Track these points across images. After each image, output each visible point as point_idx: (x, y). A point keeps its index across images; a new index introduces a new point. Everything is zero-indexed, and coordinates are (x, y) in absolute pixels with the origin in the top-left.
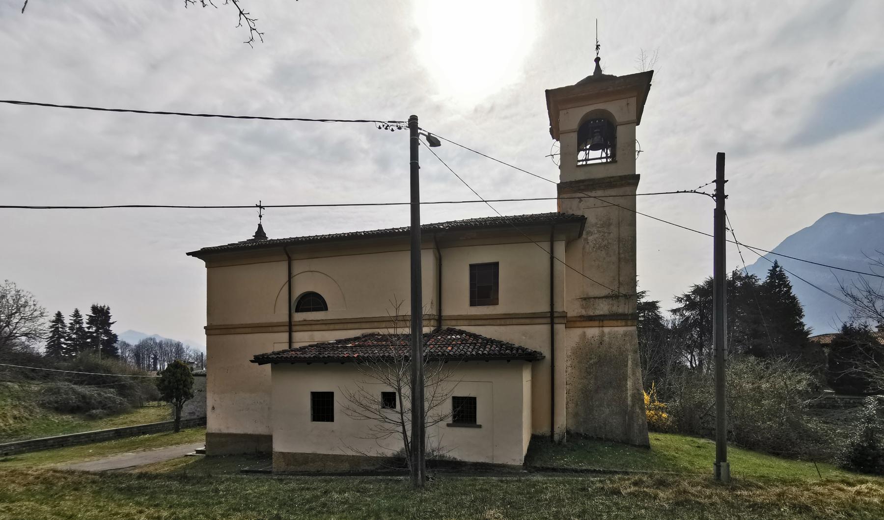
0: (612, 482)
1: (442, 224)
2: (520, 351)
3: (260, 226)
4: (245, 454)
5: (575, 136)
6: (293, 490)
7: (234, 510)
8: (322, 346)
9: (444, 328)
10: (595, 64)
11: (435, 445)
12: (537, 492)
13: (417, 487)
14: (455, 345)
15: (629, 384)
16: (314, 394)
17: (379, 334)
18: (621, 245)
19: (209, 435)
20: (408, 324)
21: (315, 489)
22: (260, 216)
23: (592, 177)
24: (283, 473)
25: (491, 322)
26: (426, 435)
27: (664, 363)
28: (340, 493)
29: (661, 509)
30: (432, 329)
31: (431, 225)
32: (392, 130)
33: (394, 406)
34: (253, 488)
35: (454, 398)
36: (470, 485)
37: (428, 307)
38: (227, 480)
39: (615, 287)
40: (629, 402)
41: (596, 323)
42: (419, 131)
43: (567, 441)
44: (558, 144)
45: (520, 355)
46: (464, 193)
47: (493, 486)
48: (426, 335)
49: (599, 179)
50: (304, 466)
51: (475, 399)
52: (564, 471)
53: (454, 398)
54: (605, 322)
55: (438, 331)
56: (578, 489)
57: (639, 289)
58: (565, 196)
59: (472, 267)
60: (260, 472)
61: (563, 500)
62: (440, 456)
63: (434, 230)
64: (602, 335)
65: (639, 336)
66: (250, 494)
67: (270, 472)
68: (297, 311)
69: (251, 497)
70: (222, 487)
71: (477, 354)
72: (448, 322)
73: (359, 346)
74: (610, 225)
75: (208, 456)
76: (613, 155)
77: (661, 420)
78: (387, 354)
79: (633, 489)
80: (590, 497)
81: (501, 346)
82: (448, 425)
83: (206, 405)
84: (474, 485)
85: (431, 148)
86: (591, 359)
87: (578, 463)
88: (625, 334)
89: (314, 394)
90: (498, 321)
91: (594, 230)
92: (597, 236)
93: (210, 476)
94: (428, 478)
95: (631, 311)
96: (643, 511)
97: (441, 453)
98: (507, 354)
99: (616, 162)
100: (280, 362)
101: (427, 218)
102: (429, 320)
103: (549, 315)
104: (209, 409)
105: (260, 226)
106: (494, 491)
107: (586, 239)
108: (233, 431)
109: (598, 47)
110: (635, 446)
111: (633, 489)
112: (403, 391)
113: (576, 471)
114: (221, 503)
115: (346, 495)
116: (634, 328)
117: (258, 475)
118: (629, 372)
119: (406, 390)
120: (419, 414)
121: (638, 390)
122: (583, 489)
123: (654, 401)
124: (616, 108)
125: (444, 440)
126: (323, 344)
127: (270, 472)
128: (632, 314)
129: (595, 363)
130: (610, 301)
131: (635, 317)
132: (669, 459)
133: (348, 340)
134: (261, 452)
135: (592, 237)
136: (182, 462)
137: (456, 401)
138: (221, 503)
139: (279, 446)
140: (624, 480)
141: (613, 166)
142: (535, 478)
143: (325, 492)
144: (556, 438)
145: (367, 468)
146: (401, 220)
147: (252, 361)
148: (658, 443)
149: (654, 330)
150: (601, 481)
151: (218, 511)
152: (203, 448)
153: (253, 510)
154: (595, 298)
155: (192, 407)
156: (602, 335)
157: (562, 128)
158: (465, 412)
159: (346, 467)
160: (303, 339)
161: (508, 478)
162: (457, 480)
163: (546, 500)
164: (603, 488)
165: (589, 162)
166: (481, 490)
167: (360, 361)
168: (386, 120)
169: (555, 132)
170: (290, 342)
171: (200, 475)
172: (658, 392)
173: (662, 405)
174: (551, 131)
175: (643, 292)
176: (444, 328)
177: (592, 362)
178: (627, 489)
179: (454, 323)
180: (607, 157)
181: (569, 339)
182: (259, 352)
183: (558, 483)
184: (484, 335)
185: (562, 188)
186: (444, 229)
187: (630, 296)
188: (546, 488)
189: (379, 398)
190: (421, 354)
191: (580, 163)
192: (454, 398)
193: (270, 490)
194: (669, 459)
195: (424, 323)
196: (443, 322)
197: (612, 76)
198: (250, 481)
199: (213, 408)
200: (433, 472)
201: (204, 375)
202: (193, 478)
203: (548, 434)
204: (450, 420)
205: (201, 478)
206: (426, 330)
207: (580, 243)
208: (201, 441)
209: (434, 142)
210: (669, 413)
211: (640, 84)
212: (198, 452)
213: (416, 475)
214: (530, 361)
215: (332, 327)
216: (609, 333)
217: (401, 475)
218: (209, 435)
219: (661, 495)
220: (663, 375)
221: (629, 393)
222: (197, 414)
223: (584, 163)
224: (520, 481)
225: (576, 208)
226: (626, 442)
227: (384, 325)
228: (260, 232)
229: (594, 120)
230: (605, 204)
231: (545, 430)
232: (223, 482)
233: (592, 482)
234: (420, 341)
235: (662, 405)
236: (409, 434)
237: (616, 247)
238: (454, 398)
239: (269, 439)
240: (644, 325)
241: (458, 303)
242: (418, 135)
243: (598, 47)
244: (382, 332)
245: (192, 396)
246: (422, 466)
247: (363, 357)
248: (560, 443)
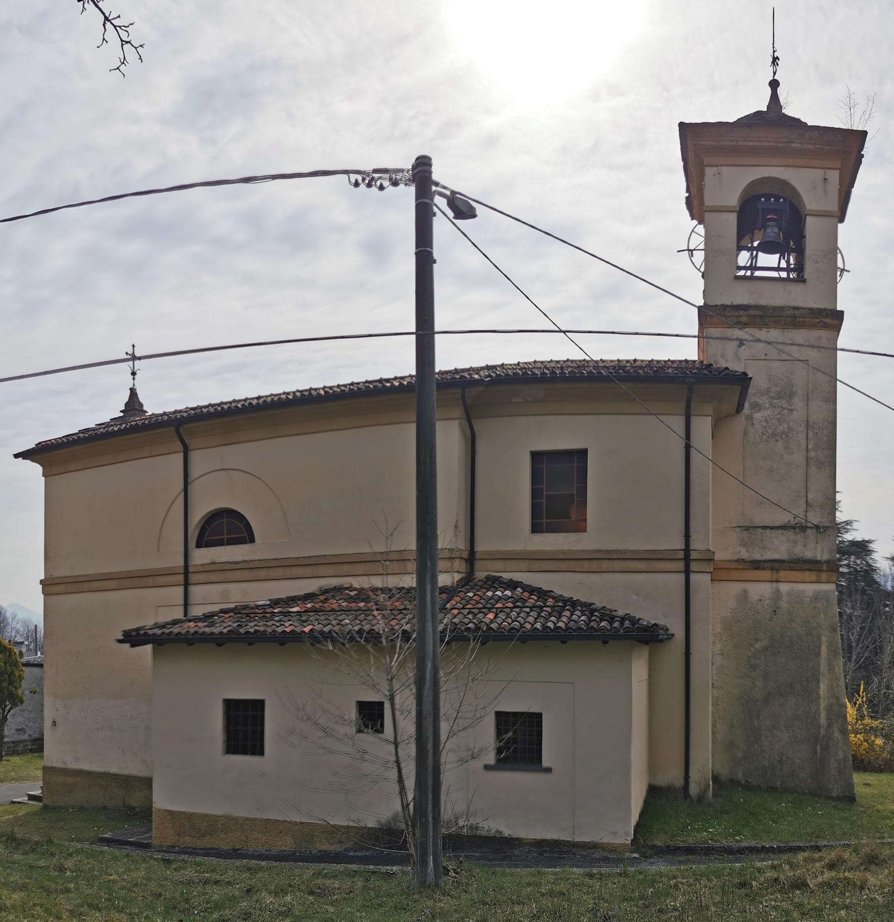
0: (793, 866)
1: (477, 370)
2: (627, 623)
3: (133, 393)
4: (105, 808)
5: (732, 219)
6: (190, 883)
7: (90, 906)
8: (242, 612)
9: (480, 575)
10: (768, 91)
11: (461, 807)
12: (657, 894)
13: (425, 886)
14: (501, 610)
15: (823, 686)
16: (229, 704)
17: (351, 588)
18: (811, 434)
19: (46, 769)
20: (412, 566)
21: (228, 883)
22: (134, 374)
23: (763, 302)
24: (171, 849)
25: (572, 565)
26: (444, 788)
27: (878, 650)
28: (276, 894)
29: (871, 905)
30: (457, 577)
31: (456, 371)
32: (381, 188)
33: (380, 730)
34: (121, 870)
35: (498, 714)
36: (529, 884)
37: (447, 537)
38: (78, 852)
39: (800, 511)
40: (823, 721)
41: (767, 574)
42: (434, 188)
43: (715, 795)
44: (701, 229)
45: (627, 630)
46: (522, 314)
47: (574, 885)
48: (443, 590)
49: (775, 308)
50: (207, 842)
51: (539, 716)
52: (709, 851)
53: (499, 715)
54: (782, 574)
55: (467, 581)
56: (734, 886)
57: (840, 517)
58: (714, 332)
59: (537, 457)
60: (131, 844)
61: (708, 908)
62: (471, 827)
63: (461, 382)
64: (777, 595)
65: (840, 601)
66: (115, 881)
67: (147, 846)
68: (199, 545)
69: (116, 887)
70: (69, 864)
71: (545, 627)
72: (489, 564)
73: (315, 610)
74: (792, 395)
75: (45, 807)
76: (799, 268)
77: (874, 750)
78: (367, 627)
79: (828, 875)
80: (753, 898)
81: (592, 612)
82: (487, 767)
83: (42, 719)
84: (538, 884)
85: (455, 221)
86: (757, 640)
87: (733, 836)
88: (817, 597)
89: (229, 704)
90: (586, 565)
91: (764, 401)
92: (769, 412)
93: (50, 842)
94: (446, 871)
95: (826, 557)
96: (843, 912)
97: (472, 821)
98: (604, 628)
99: (804, 281)
100: (163, 641)
101: (450, 356)
102: (451, 559)
103: (681, 555)
104: (47, 724)
105: (133, 393)
106: (575, 895)
107: (750, 418)
108: (85, 766)
109: (775, 60)
110: (832, 798)
111: (828, 875)
112: (397, 699)
113: (729, 851)
114: (68, 891)
115: (288, 898)
116: (831, 587)
117: (129, 849)
118: (823, 666)
119: (406, 699)
120: (430, 746)
121: (837, 698)
122: (743, 885)
123: (862, 717)
124: (808, 183)
125: (478, 794)
126: (246, 607)
127: (147, 846)
128: (828, 562)
129: (765, 649)
130: (790, 534)
131: (832, 567)
132: (884, 818)
133: (293, 600)
134: (133, 808)
135: (760, 414)
136: (6, 812)
137: (503, 720)
138: (68, 891)
139: (162, 800)
140: (814, 861)
141: (800, 287)
142: (653, 869)
143: (249, 891)
144: (694, 790)
145: (326, 847)
146: (398, 361)
147: (119, 641)
148: (868, 790)
149: (863, 592)
150: (774, 867)
151: (65, 904)
152: (37, 792)
153: (121, 910)
154: (765, 527)
155: (21, 719)
156: (777, 595)
157: (710, 200)
158: (520, 741)
159: (286, 844)
160: (208, 598)
161: (604, 870)
162: (504, 875)
163: (675, 909)
164: (776, 880)
165: (758, 273)
166: (551, 893)
167: (315, 638)
168: (369, 168)
169: (696, 206)
170: (186, 605)
171: (36, 838)
172: (870, 701)
173: (876, 723)
174: (689, 202)
175: (848, 523)
176: (480, 575)
177: (758, 645)
178: (818, 875)
179: (499, 565)
180: (788, 270)
181: (717, 600)
182: (132, 625)
183: (697, 877)
184: (558, 591)
185: (708, 315)
186: (480, 382)
187: (826, 528)
188: (676, 885)
189: (352, 714)
190: (434, 627)
191: (742, 273)
192: (498, 714)
193: (149, 879)
194: (884, 818)
195: (441, 565)
196: (478, 565)
197: (799, 121)
198: (115, 859)
199: (54, 723)
200: (457, 857)
201: (41, 666)
202: (25, 841)
203: (679, 782)
204: (491, 758)
205: (37, 843)
206: (444, 580)
207: (739, 423)
208: (35, 779)
209: (463, 209)
210: (886, 737)
211: (843, 150)
212: (32, 798)
213: (424, 864)
214: (647, 644)
215: (262, 573)
216: (789, 594)
217: (393, 864)
218: (46, 769)
219: (872, 880)
220: (878, 671)
221: (823, 704)
222: (29, 732)
223: (749, 273)
224: (623, 874)
225: (730, 358)
226: (818, 793)
227: (361, 568)
228: (133, 404)
229: (768, 197)
230: (784, 356)
231: (672, 776)
232: (71, 855)
233: (759, 870)
234: (433, 602)
235: (876, 723)
236: (410, 784)
237: (802, 437)
238: (499, 715)
239: (147, 783)
240: (849, 581)
241: (509, 523)
242: (431, 196)
243: (775, 60)
244: (356, 582)
245: (22, 702)
246: (435, 845)
247: (322, 632)
248: (701, 798)
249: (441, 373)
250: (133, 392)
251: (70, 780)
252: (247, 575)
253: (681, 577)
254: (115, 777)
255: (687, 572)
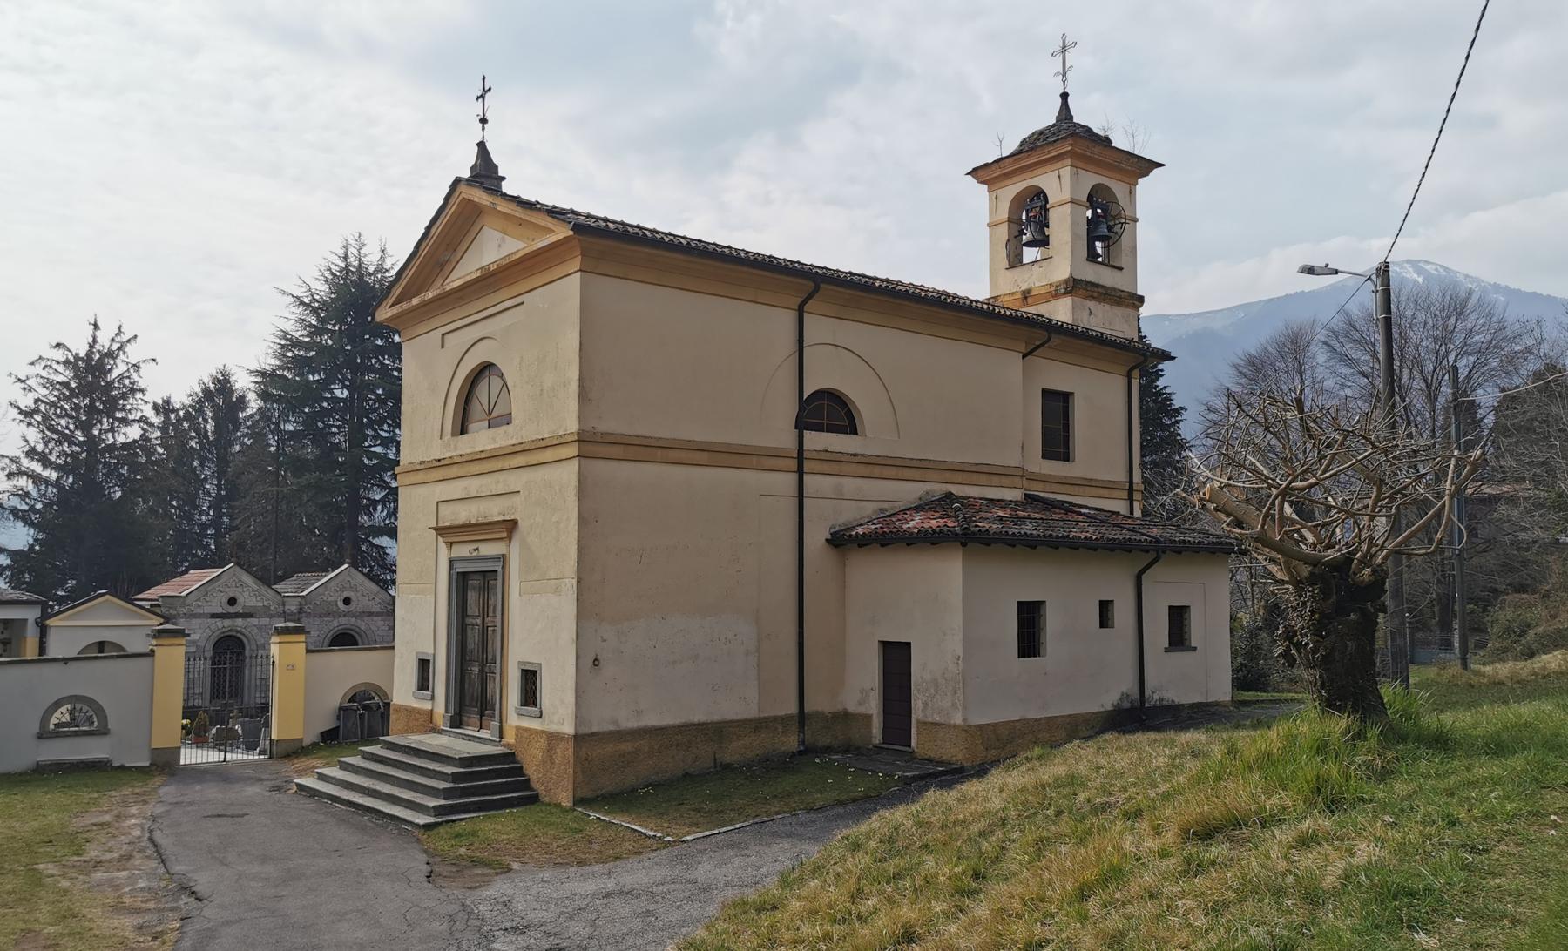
10: (1059, 101)
108: (652, 720)
215: (877, 471)
249: (1271, 372)
250: (482, 145)
251: (626, 747)
252: (862, 470)
253: (795, 477)
254: (700, 727)
255: (800, 472)
